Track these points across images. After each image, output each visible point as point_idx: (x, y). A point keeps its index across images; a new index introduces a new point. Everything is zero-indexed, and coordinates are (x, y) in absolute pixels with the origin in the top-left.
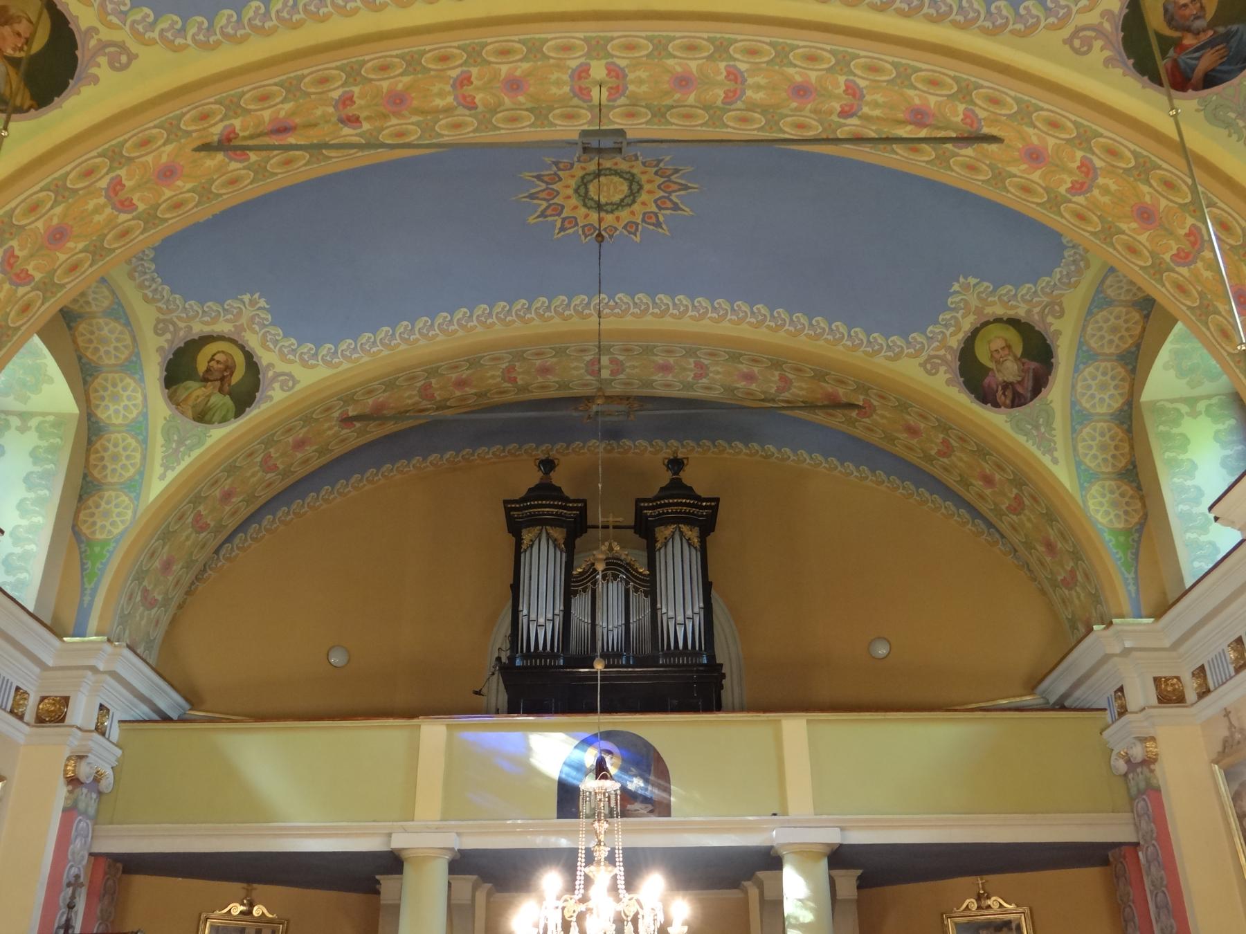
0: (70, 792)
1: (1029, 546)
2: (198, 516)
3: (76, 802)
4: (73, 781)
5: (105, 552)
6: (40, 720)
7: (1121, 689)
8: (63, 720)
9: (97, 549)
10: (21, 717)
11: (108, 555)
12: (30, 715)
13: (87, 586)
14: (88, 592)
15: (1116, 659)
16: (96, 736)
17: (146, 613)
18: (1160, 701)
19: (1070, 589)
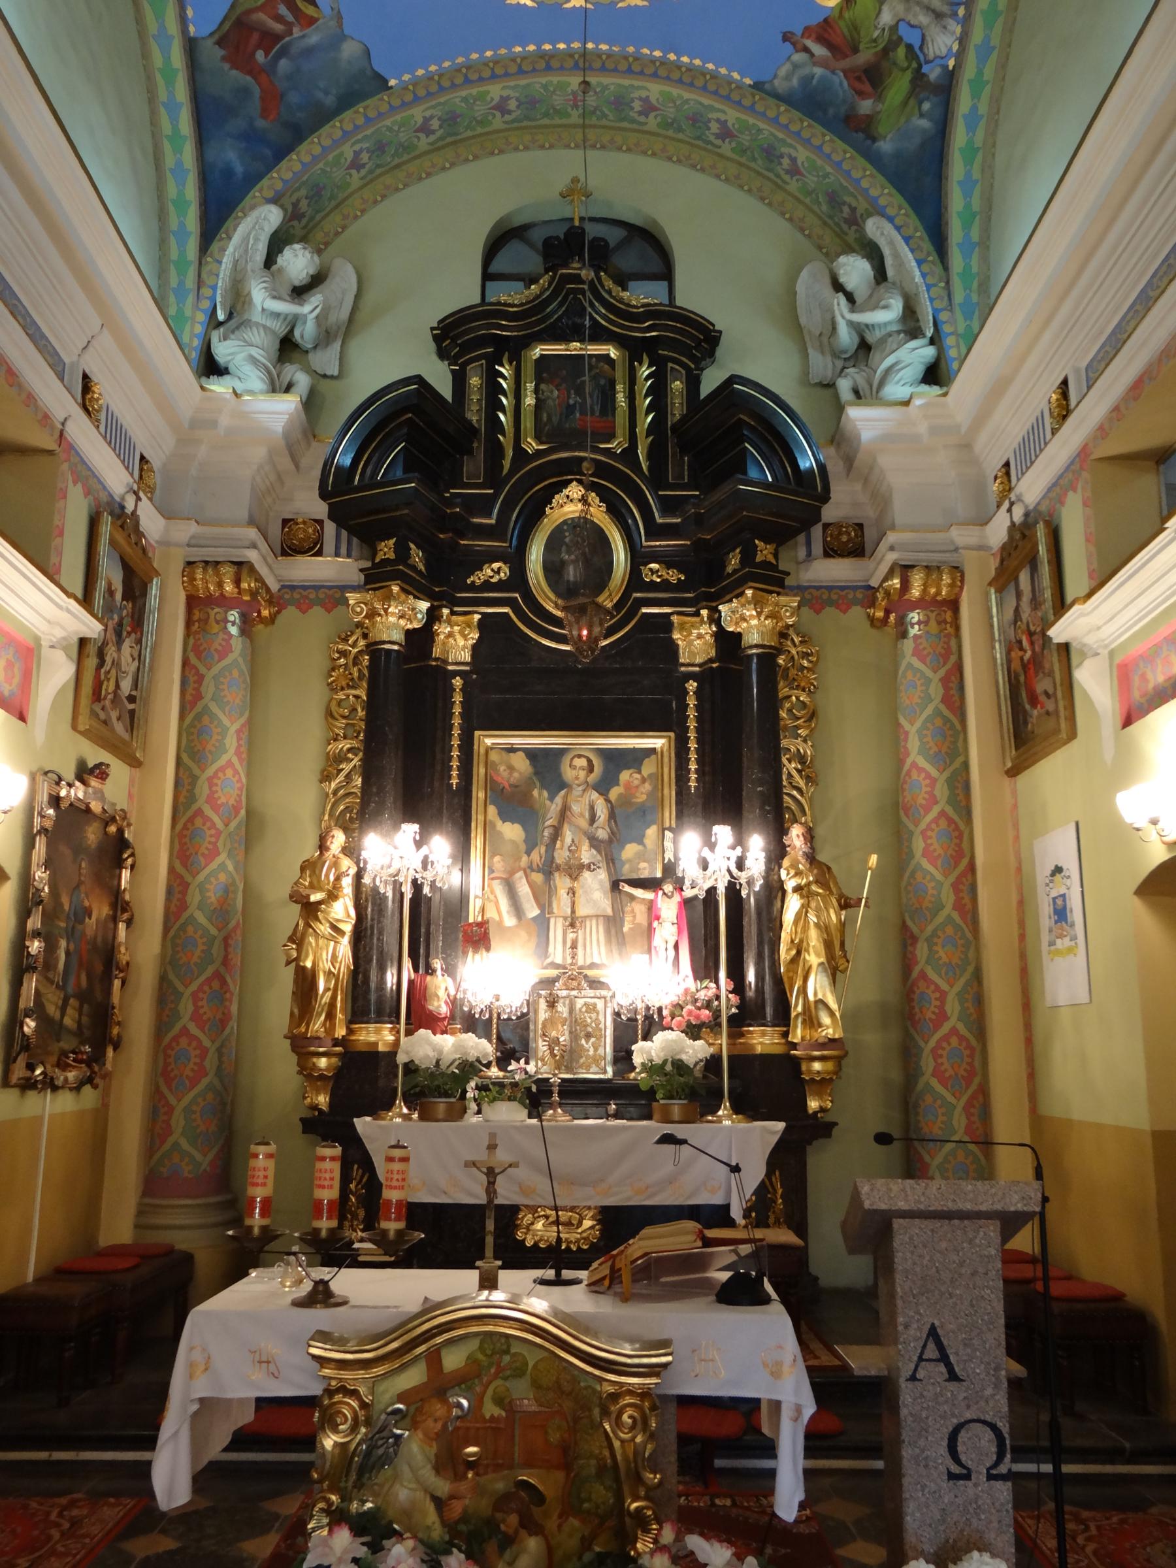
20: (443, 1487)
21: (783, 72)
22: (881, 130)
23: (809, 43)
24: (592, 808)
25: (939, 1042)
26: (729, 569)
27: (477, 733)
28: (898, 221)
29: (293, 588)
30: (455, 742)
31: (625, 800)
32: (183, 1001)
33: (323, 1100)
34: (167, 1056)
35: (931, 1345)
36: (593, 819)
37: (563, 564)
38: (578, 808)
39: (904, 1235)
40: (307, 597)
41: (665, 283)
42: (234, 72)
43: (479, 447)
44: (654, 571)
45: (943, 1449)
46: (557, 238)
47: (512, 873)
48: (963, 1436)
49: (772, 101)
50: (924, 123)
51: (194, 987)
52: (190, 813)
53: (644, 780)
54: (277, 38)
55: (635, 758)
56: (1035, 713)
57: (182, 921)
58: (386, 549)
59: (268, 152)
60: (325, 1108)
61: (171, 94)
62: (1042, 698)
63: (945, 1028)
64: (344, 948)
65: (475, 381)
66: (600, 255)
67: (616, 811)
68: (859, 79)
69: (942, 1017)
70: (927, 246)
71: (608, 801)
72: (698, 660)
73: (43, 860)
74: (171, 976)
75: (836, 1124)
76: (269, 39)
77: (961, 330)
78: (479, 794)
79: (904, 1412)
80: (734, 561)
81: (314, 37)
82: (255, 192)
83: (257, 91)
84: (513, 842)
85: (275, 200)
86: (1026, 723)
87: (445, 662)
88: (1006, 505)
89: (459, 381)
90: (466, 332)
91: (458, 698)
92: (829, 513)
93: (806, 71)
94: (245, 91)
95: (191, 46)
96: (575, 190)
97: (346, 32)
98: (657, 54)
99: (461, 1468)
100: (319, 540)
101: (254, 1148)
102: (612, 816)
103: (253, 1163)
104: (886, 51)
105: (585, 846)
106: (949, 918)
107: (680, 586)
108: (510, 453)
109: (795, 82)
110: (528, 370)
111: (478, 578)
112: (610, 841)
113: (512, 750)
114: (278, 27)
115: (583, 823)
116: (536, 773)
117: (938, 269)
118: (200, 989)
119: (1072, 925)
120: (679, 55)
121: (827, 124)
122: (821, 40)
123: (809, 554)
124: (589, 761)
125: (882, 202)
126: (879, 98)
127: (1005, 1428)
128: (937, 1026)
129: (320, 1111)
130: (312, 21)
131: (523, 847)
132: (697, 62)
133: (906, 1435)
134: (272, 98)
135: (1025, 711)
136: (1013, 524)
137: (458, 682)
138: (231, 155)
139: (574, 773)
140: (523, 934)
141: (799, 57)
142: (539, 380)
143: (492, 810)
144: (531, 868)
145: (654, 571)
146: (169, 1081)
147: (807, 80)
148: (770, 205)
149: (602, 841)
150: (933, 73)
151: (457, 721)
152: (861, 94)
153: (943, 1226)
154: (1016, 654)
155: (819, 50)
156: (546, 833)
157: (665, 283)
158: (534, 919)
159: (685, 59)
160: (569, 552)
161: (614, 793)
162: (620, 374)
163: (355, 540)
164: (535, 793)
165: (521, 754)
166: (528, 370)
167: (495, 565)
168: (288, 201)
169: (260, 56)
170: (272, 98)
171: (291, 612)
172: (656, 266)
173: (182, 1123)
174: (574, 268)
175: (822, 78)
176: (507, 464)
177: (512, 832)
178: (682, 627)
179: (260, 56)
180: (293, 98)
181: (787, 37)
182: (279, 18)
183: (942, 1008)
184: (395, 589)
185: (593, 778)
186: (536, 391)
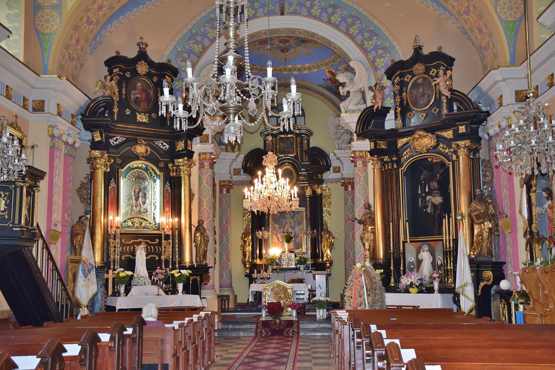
0: (52, 140)
1: (471, 30)
2: (88, 18)
3: (54, 144)
4: (52, 136)
5: (51, 39)
6: (35, 110)
7: (501, 96)
8: (44, 111)
9: (47, 37)
10: (27, 109)
11: (52, 40)
12: (30, 109)
13: (45, 54)
14: (46, 57)
15: (500, 83)
16: (59, 117)
17: (87, 27)
18: (516, 101)
19: (487, 51)
24: (291, 221)
29: (236, 182)
33: (248, 271)
41: (303, 117)
64: (250, 247)
69: (350, 256)
73: (211, 270)
100: (240, 172)
118: (207, 177)
122: (329, 81)
144: (280, 232)
146: (222, 269)
147: (328, 86)
155: (330, 82)
157: (303, 117)
161: (295, 218)
181: (323, 79)
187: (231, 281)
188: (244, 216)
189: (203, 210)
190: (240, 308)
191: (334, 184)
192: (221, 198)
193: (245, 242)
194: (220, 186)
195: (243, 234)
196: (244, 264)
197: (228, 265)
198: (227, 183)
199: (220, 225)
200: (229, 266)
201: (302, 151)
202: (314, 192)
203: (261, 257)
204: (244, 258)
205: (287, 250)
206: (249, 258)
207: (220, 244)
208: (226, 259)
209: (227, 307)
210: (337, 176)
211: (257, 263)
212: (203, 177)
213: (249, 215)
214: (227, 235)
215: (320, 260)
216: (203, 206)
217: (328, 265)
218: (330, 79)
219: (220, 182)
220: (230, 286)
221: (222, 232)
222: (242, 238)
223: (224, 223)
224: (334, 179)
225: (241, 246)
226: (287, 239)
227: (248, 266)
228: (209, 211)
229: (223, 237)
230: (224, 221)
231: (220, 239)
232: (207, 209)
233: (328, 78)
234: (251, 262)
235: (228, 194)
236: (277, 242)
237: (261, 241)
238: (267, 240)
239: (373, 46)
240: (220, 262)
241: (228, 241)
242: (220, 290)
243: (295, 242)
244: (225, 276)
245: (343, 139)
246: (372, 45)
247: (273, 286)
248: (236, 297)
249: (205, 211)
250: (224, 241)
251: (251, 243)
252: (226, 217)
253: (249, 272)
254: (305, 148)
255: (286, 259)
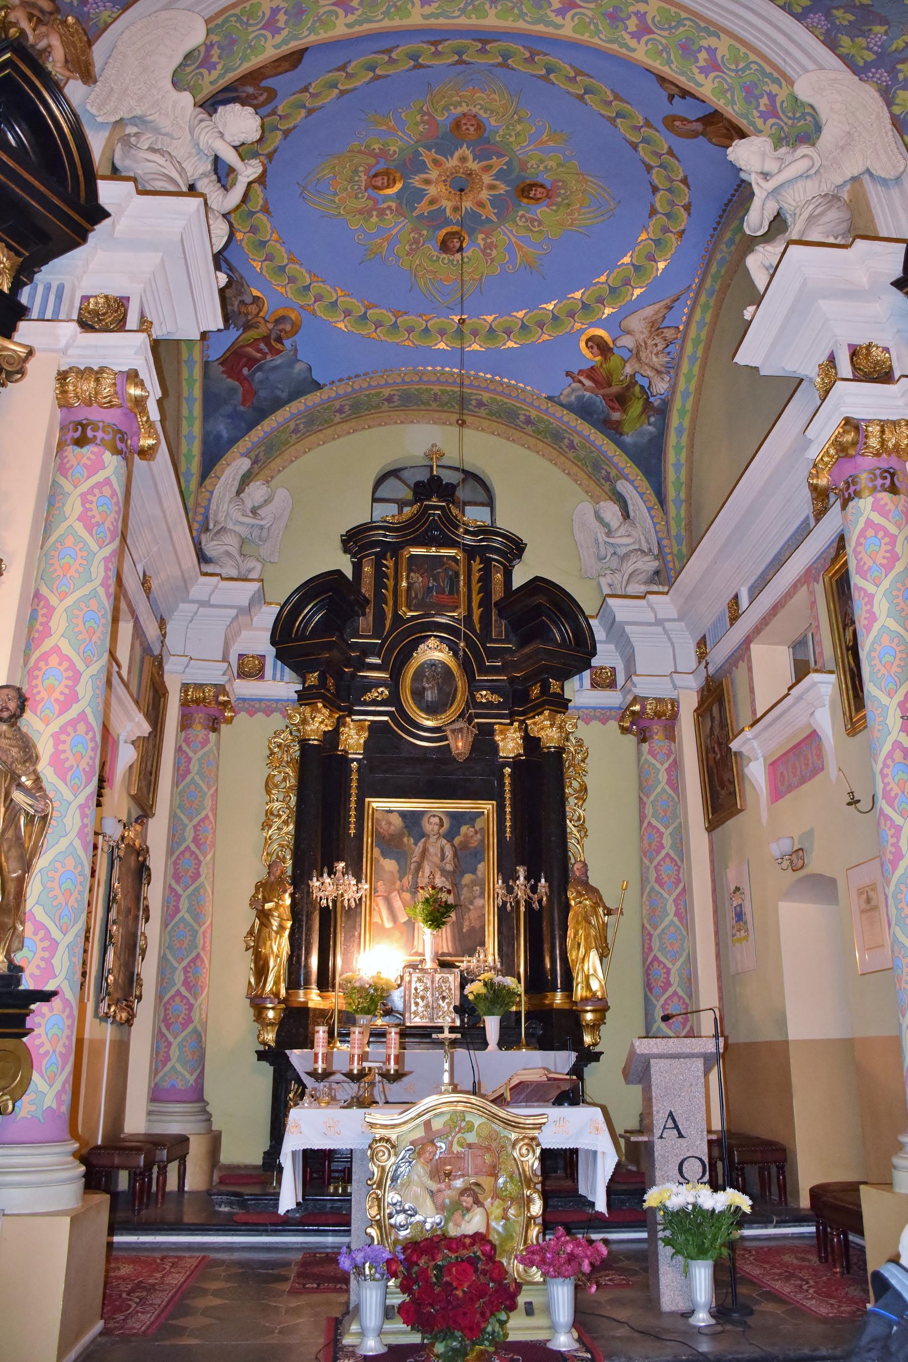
20: (434, 1186)
21: (565, 392)
22: (626, 429)
23: (582, 378)
24: (442, 850)
25: (666, 1000)
26: (533, 696)
27: (367, 800)
28: (636, 484)
29: (244, 700)
30: (353, 805)
31: (464, 845)
32: (177, 973)
33: (270, 1037)
34: (166, 1009)
35: (670, 1121)
36: (443, 858)
37: (424, 689)
38: (433, 850)
39: (656, 1066)
40: (253, 706)
41: (489, 509)
42: (229, 380)
43: (370, 610)
44: (484, 696)
45: (676, 1171)
46: (423, 482)
47: (390, 893)
48: (685, 1164)
49: (558, 408)
50: (651, 428)
51: (184, 964)
52: (182, 849)
53: (476, 832)
54: (257, 360)
55: (470, 818)
56: (723, 792)
57: (177, 919)
58: (313, 678)
59: (243, 425)
60: (273, 1044)
61: (191, 392)
62: (727, 784)
63: (670, 991)
65: (367, 569)
66: (447, 492)
67: (459, 853)
68: (611, 400)
69: (668, 984)
70: (654, 499)
71: (453, 845)
72: (512, 755)
74: (169, 956)
75: (602, 1053)
76: (251, 362)
77: (675, 552)
78: (367, 840)
79: (656, 1154)
80: (536, 691)
81: (279, 360)
82: (234, 449)
83: (241, 390)
84: (392, 872)
85: (246, 455)
86: (718, 798)
87: (347, 752)
88: (704, 663)
89: (357, 568)
90: (362, 539)
91: (354, 777)
92: (595, 662)
93: (580, 393)
94: (233, 390)
95: (206, 365)
96: (435, 453)
97: (299, 357)
98: (489, 376)
99: (443, 1177)
100: (262, 669)
101: (317, 1028)
102: (455, 855)
103: (316, 1035)
104: (628, 388)
105: (438, 876)
106: (672, 922)
107: (499, 706)
108: (389, 616)
109: (573, 398)
110: (404, 565)
111: (368, 697)
112: (454, 872)
113: (390, 812)
114: (259, 355)
115: (437, 860)
116: (406, 827)
117: (661, 513)
119: (746, 923)
120: (502, 378)
121: (593, 424)
122: (589, 377)
123: (581, 686)
124: (441, 819)
125: (626, 471)
126: (625, 411)
127: (706, 1161)
128: (665, 990)
129: (269, 1046)
130: (279, 352)
131: (397, 875)
132: (513, 382)
133: (657, 1165)
134: (249, 393)
135: (718, 792)
136: (708, 676)
137: (354, 765)
138: (222, 428)
139: (431, 827)
140: (397, 933)
141: (575, 385)
142: (410, 570)
143: (377, 851)
145: (484, 696)
146: (168, 1027)
147: (580, 398)
148: (556, 464)
149: (449, 872)
150: (656, 402)
151: (354, 791)
152: (613, 409)
153: (675, 1062)
154: (711, 756)
155: (588, 383)
156: (412, 867)
158: (405, 923)
159: (505, 380)
160: (428, 682)
161: (457, 840)
162: (462, 569)
163: (287, 669)
164: (405, 839)
165: (396, 814)
166: (404, 565)
167: (381, 689)
168: (253, 454)
169: (245, 371)
170: (249, 393)
171: (243, 715)
172: (483, 497)
173: (177, 1053)
174: (434, 501)
175: (590, 398)
176: (388, 623)
177: (390, 865)
178: (502, 732)
179: (245, 371)
180: (262, 394)
181: (568, 374)
182: (259, 351)
183: (668, 978)
184: (320, 705)
185: (443, 830)
186: (408, 577)
187: (201, 1075)
188: (267, 825)
189: (44, 657)
190: (230, 1204)
191: (595, 724)
192: (185, 748)
193: (264, 916)
194: (184, 704)
195: (257, 888)
196: (257, 1004)
197: (191, 1007)
198: (209, 693)
199: (170, 851)
200: (196, 1015)
201: (485, 603)
202: (531, 743)
203: (325, 982)
204: (258, 982)
205: (428, 956)
206: (277, 983)
207: (165, 924)
208: (186, 983)
209: (172, 1184)
210: (612, 698)
211: (311, 1005)
212: (67, 486)
213: (286, 823)
214: (197, 890)
215: (558, 999)
216: (47, 632)
217: (589, 1016)
218: (591, 373)
219: (185, 687)
220: (197, 1095)
221: (177, 877)
222: (253, 902)
223: (189, 842)
224: (595, 709)
225: (251, 933)
226: (430, 914)
227: (271, 1014)
228: (80, 665)
229: (178, 897)
230: (189, 833)
231: (166, 902)
232: (66, 649)
233: (586, 366)
234: (285, 1001)
235: (213, 736)
236: (388, 924)
237: (328, 916)
238: (353, 913)
239: (875, 53)
240: (159, 996)
241: (197, 913)
242: (150, 1113)
243: (458, 925)
244: (174, 1052)
245: (630, 571)
246: (869, 49)
247: (428, 1124)
248: (215, 1142)
249: (54, 660)
250: (183, 913)
251: (289, 924)
252: (195, 822)
253: (277, 1042)
254: (498, 593)
255: (426, 989)
